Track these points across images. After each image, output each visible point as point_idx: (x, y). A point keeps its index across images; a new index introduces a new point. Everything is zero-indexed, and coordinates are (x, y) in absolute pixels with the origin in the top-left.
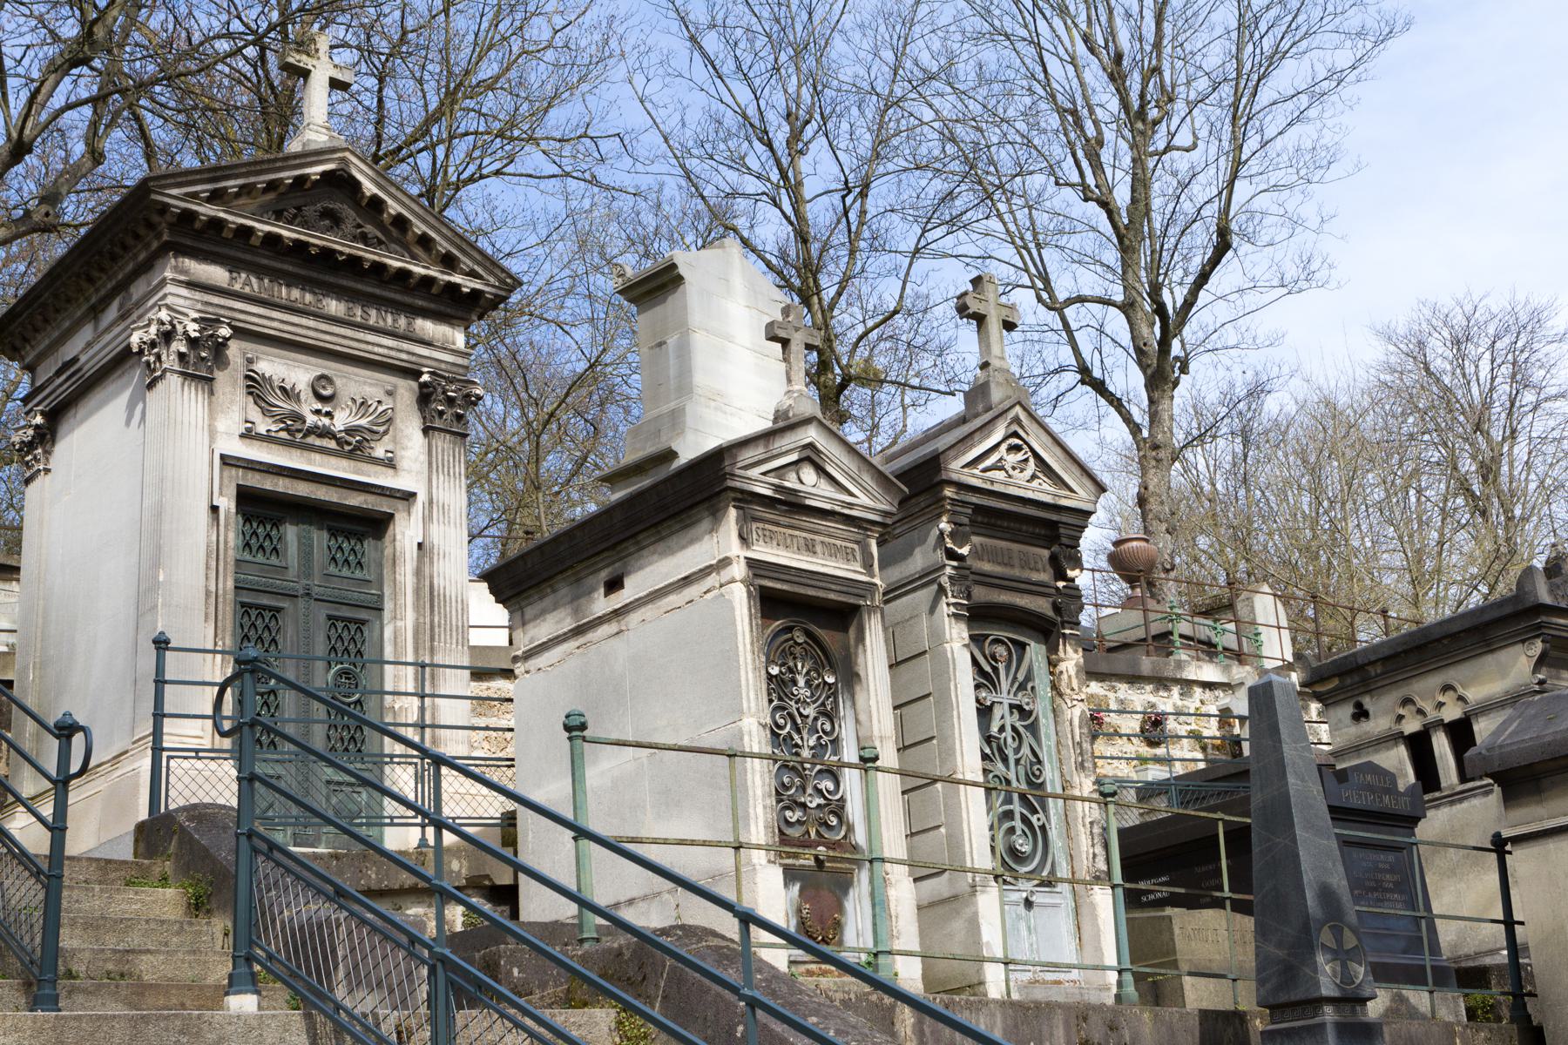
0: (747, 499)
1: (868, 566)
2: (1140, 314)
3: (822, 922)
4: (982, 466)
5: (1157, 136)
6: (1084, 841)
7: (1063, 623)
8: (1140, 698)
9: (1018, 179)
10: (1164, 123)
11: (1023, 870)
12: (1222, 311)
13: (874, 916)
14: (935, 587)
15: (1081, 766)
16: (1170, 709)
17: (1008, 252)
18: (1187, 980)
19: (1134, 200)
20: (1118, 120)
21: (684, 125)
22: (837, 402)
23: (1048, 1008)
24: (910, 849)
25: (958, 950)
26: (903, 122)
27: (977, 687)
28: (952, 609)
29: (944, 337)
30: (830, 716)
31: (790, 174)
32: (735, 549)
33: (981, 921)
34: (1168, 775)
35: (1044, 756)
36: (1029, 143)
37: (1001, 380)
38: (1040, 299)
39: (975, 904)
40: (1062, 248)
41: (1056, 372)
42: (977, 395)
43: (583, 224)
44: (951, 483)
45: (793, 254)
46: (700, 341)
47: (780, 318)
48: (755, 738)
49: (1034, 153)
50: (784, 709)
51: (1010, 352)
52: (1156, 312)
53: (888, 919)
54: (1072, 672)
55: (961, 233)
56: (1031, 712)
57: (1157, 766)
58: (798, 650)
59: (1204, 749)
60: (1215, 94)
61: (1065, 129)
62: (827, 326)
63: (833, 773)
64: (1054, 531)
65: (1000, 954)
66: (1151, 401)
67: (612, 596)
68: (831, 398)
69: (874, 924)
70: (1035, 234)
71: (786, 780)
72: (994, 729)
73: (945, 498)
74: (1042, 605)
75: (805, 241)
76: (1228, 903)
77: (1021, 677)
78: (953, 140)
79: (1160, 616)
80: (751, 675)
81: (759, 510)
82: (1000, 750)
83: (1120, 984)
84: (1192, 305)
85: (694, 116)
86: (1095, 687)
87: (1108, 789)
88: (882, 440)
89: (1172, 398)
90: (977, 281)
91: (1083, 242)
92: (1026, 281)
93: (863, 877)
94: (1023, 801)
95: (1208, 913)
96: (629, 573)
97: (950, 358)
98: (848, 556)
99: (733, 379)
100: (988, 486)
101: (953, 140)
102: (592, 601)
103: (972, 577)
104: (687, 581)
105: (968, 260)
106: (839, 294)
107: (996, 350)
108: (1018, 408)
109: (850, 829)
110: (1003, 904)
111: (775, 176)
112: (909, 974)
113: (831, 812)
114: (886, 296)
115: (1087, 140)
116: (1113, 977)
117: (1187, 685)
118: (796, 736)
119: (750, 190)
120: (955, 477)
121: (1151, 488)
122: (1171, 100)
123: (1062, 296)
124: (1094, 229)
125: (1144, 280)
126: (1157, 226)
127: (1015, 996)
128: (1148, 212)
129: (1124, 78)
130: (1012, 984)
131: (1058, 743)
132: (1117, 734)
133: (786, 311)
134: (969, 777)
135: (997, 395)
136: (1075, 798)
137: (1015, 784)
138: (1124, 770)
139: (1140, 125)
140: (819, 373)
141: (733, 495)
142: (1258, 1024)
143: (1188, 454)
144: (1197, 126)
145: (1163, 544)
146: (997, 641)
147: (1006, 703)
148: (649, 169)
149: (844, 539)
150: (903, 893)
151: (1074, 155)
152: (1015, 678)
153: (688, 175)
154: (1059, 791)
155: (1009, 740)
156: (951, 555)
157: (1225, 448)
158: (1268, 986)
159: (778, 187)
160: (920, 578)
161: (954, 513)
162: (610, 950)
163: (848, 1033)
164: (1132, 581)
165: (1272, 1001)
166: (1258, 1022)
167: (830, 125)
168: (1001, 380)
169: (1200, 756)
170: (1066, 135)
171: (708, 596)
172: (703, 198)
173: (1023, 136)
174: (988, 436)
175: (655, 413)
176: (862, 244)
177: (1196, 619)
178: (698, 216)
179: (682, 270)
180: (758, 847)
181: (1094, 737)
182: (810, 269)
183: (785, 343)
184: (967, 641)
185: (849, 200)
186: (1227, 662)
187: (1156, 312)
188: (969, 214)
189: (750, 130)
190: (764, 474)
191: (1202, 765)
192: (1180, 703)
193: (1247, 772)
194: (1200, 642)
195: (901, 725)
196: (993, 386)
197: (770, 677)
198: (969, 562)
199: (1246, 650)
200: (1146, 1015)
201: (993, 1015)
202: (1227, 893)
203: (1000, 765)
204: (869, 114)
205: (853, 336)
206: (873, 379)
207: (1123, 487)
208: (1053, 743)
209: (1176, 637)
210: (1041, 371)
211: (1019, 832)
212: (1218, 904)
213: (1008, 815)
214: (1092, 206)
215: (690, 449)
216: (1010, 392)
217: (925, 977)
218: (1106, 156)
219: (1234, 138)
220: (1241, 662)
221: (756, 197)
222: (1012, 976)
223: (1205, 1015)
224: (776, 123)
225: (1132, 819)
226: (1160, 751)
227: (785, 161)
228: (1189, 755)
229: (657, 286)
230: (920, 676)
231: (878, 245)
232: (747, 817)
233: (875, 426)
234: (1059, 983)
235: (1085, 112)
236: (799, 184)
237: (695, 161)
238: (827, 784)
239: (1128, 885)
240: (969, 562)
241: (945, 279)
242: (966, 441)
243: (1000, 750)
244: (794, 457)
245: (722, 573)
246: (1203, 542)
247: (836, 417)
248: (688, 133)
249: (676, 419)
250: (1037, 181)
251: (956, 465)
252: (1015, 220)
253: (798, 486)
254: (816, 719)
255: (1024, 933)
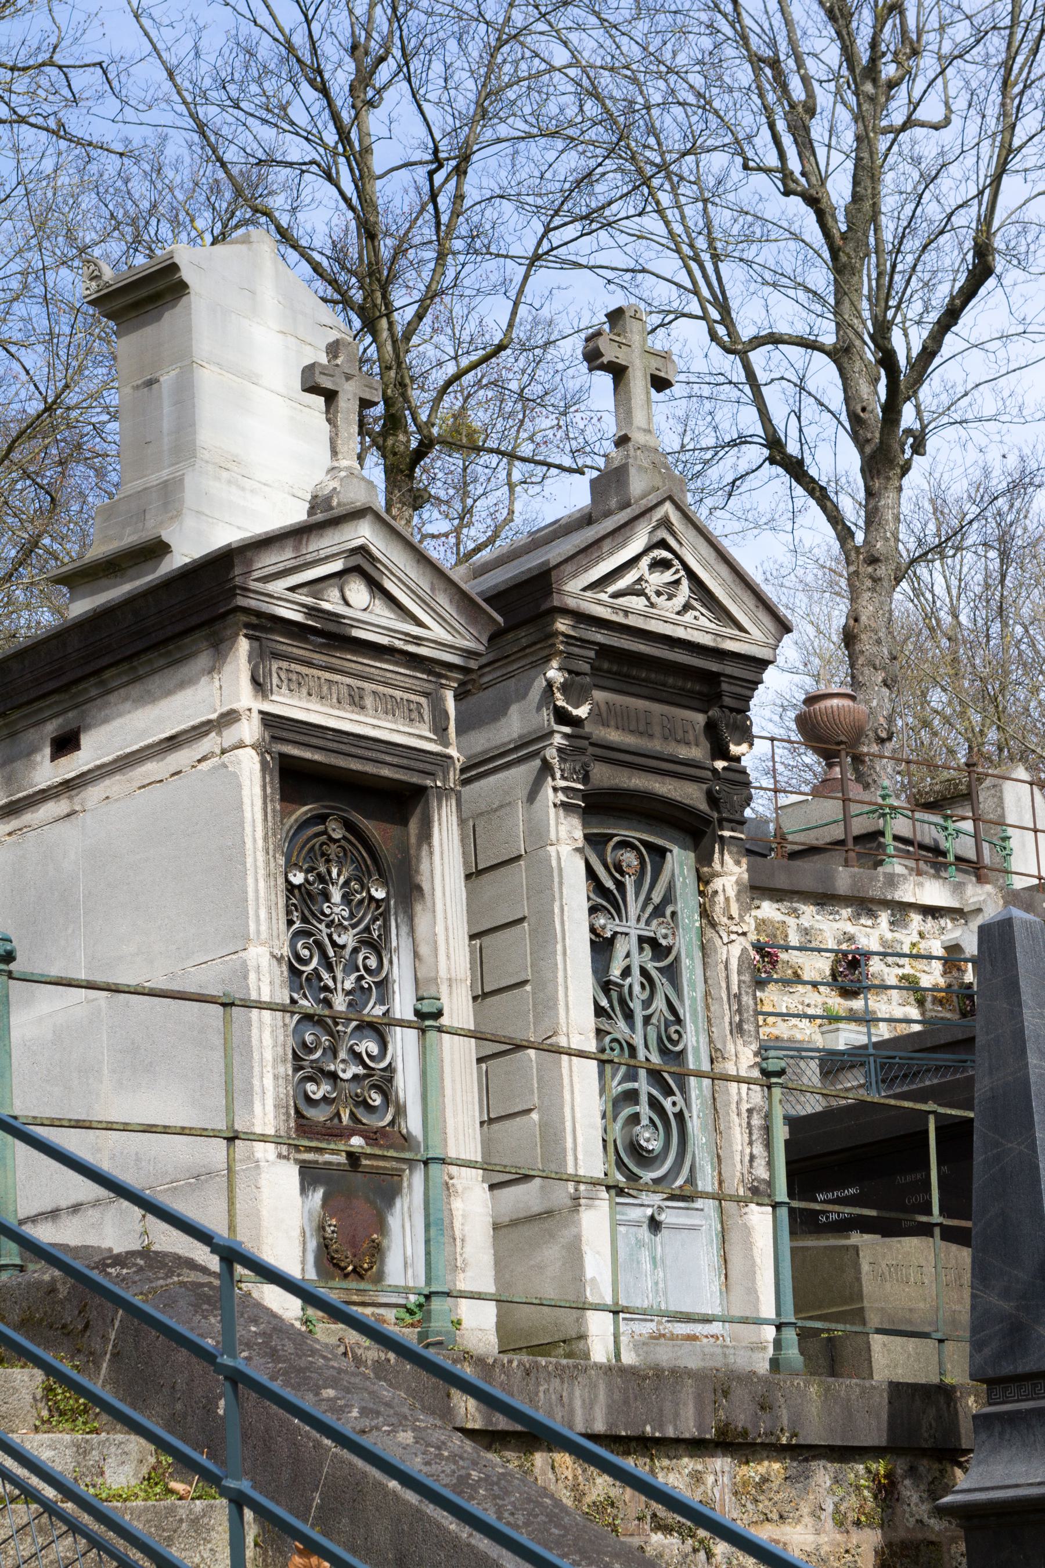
0: (265, 626)
1: (440, 730)
2: (858, 365)
3: (353, 1243)
4: (611, 589)
5: (893, 105)
6: (738, 1137)
7: (721, 821)
8: (832, 927)
9: (690, 159)
10: (904, 86)
11: (648, 1176)
12: (977, 366)
13: (427, 1242)
14: (537, 763)
15: (738, 1029)
16: (875, 946)
17: (670, 265)
18: (877, 1341)
19: (856, 198)
20: (838, 77)
21: (197, 55)
22: (411, 476)
23: (678, 1374)
24: (487, 1145)
25: (550, 1292)
26: (523, 66)
27: (593, 910)
28: (561, 797)
29: (573, 385)
30: (377, 946)
31: (354, 135)
32: (245, 698)
33: (585, 1248)
34: (863, 1040)
35: (685, 1012)
36: (705, 104)
37: (646, 464)
38: (714, 336)
39: (578, 1224)
40: (749, 263)
41: (733, 444)
42: (610, 483)
43: (43, 192)
44: (566, 612)
45: (353, 252)
46: (209, 380)
47: (323, 359)
48: (267, 982)
49: (714, 122)
50: (310, 934)
51: (663, 421)
52: (881, 362)
53: (452, 1249)
54: (732, 893)
55: (602, 233)
56: (669, 949)
57: (853, 1026)
58: (333, 850)
59: (921, 1003)
60: (979, 48)
61: (759, 87)
62: (399, 364)
63: (378, 1029)
64: (713, 687)
65: (609, 1300)
66: (869, 493)
67: (63, 760)
68: (402, 470)
69: (428, 1253)
70: (711, 241)
71: (309, 1038)
72: (615, 972)
73: (557, 633)
74: (691, 795)
75: (371, 236)
76: (937, 1231)
77: (657, 897)
78: (595, 94)
79: (867, 808)
80: (262, 884)
81: (282, 642)
82: (623, 1002)
83: (778, 1344)
84: (933, 354)
85: (214, 42)
86: (768, 910)
87: (773, 1065)
88: (476, 533)
89: (900, 489)
90: (616, 316)
91: (782, 255)
92: (695, 308)
93: (416, 1181)
94: (651, 1080)
95: (911, 1244)
96: (88, 727)
97: (577, 419)
98: (412, 714)
99: (255, 450)
100: (619, 618)
101: (595, 94)
102: (33, 766)
103: (591, 750)
104: (173, 742)
105: (609, 274)
106: (419, 316)
107: (639, 418)
108: (668, 506)
109: (401, 1111)
110: (615, 1224)
111: (331, 137)
112: (478, 1325)
113: (374, 1086)
114: (488, 321)
115: (792, 106)
116: (769, 1333)
117: (901, 909)
118: (325, 975)
119: (293, 157)
120: (572, 603)
121: (863, 619)
122: (915, 53)
123: (746, 332)
124: (797, 237)
125: (866, 314)
126: (888, 236)
127: (628, 1358)
128: (875, 214)
129: (848, 16)
130: (624, 1340)
131: (707, 994)
132: (797, 979)
133: (333, 349)
134: (576, 1044)
135: (637, 484)
136: (727, 1078)
137: (641, 1053)
138: (806, 1032)
139: (869, 88)
140: (385, 433)
141: (244, 618)
142: (972, 1405)
143: (922, 570)
144: (952, 93)
145: (878, 700)
146: (624, 844)
147: (634, 934)
148: (145, 117)
149: (407, 690)
150: (473, 1205)
151: (772, 126)
152: (648, 899)
153: (201, 128)
154: (706, 1066)
155: (637, 988)
156: (562, 717)
157: (973, 565)
158: (987, 1351)
159: (336, 154)
160: (516, 749)
161: (570, 656)
162: (38, 1284)
163: (378, 1413)
164: (829, 756)
165: (990, 1373)
166: (971, 1400)
167: (415, 64)
168: (646, 464)
169: (914, 1013)
170: (761, 96)
171: (204, 766)
172: (223, 165)
173: (699, 95)
174: (623, 545)
175: (137, 485)
176: (458, 245)
177: (918, 815)
178: (216, 188)
179: (187, 274)
180: (263, 1138)
181: (760, 984)
182: (378, 279)
183: (330, 396)
184: (580, 843)
185: (439, 178)
186: (960, 877)
187: (881, 362)
188: (614, 207)
189: (296, 67)
190: (292, 589)
191: (917, 1028)
192: (889, 936)
193: (972, 1040)
194: (922, 847)
195: (480, 963)
196: (632, 471)
197: (291, 888)
198: (588, 728)
199: (987, 860)
200: (813, 1389)
201: (594, 1386)
202: (936, 1217)
203: (622, 1024)
204: (475, 49)
205: (439, 377)
206: (465, 442)
207: (818, 616)
208: (699, 994)
209: (888, 839)
210: (711, 441)
211: (645, 1121)
212: (925, 1231)
213: (631, 1096)
214: (796, 203)
215: (188, 546)
216: (658, 482)
217: (500, 1326)
218: (818, 130)
219: (1004, 114)
220: (980, 880)
221: (302, 167)
222: (623, 1327)
223: (897, 1389)
224: (335, 58)
225: (811, 1105)
226: (857, 1004)
227: (346, 116)
228: (899, 1012)
229: (148, 296)
230: (511, 890)
231: (480, 245)
232: (249, 1091)
233: (468, 511)
234: (693, 1338)
235: (791, 63)
236: (366, 150)
237: (213, 110)
238: (369, 1046)
239: (795, 1204)
240: (588, 728)
241: (575, 301)
242: (591, 551)
243: (623, 1002)
244: (337, 566)
245: (226, 733)
246: (937, 698)
247: (409, 499)
248: (204, 68)
249: (169, 496)
250: (716, 162)
251: (574, 586)
252: (683, 217)
253: (341, 609)
254: (355, 951)
255: (647, 1266)
